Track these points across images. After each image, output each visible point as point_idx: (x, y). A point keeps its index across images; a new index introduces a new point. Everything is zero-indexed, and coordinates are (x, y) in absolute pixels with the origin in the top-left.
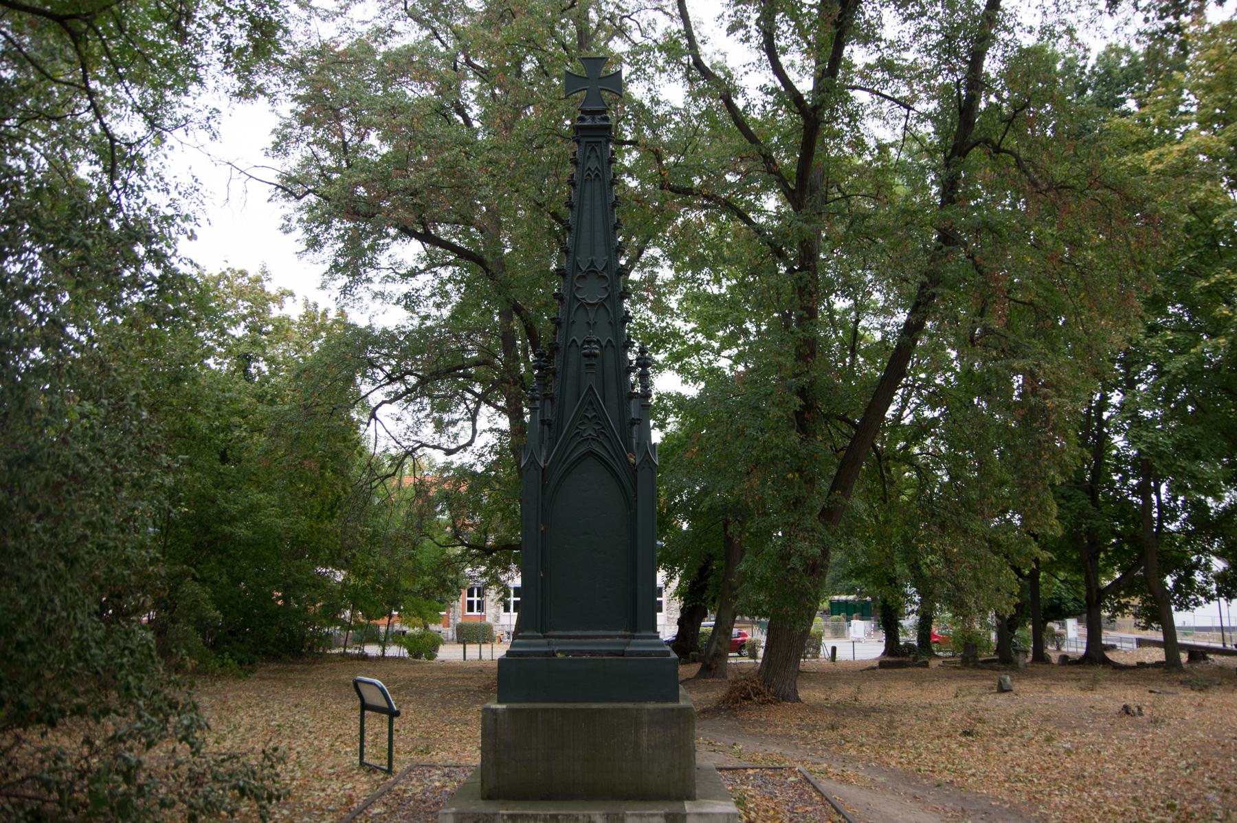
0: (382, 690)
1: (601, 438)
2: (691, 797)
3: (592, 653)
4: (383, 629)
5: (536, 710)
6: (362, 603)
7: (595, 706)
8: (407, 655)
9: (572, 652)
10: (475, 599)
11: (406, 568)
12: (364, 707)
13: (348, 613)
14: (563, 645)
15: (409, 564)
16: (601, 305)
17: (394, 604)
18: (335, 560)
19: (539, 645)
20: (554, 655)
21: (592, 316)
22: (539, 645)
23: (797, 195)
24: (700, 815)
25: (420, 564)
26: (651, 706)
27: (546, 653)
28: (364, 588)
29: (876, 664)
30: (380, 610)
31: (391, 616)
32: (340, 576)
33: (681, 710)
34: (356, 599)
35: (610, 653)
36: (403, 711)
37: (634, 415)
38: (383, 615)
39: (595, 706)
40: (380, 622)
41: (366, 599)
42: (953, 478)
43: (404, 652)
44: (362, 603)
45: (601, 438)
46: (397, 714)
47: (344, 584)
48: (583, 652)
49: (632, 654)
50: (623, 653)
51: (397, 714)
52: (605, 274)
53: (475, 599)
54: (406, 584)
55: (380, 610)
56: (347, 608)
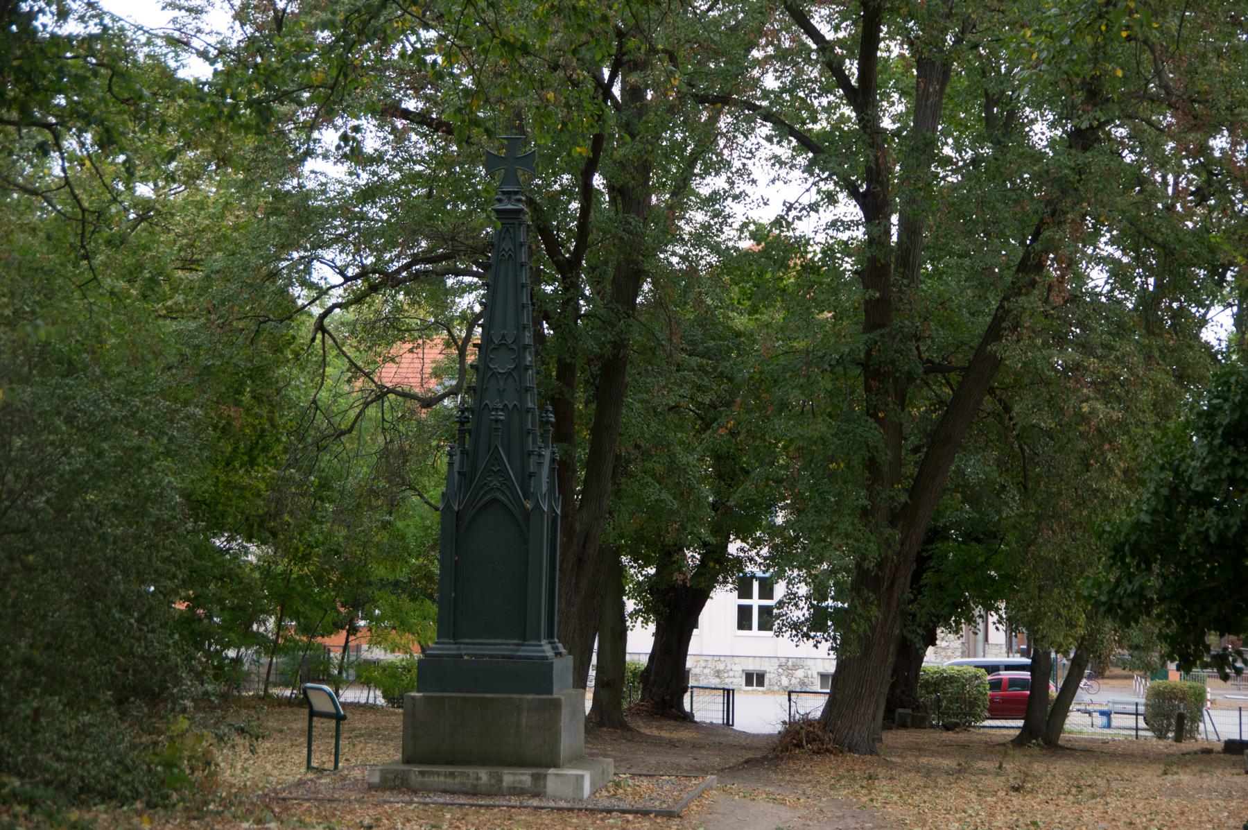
0: (330, 695)
1: (504, 488)
2: (556, 766)
3: (491, 656)
4: (336, 655)
5: (444, 698)
6: (298, 605)
7: (488, 695)
8: (381, 701)
9: (475, 655)
10: (755, 602)
11: (378, 545)
12: (313, 714)
13: (271, 622)
14: (469, 649)
15: (383, 537)
16: (509, 374)
17: (357, 604)
18: (253, 529)
19: (450, 649)
20: (461, 656)
21: (502, 383)
22: (450, 649)
23: (860, 99)
24: (557, 775)
25: (403, 538)
26: (530, 697)
27: (455, 656)
28: (301, 578)
29: (1219, 747)
30: (331, 616)
31: (353, 630)
32: (254, 554)
33: (552, 700)
34: (287, 598)
35: (504, 657)
36: (349, 715)
37: (532, 470)
38: (337, 627)
39: (488, 695)
40: (327, 641)
41: (306, 597)
42: (298, 620)
43: (377, 697)
44: (298, 605)
45: (504, 488)
46: (344, 718)
47: (266, 571)
48: (484, 656)
49: (520, 657)
50: (512, 657)
51: (344, 718)
52: (514, 347)
53: (755, 602)
54: (380, 571)
55: (331, 616)
56: (269, 613)
